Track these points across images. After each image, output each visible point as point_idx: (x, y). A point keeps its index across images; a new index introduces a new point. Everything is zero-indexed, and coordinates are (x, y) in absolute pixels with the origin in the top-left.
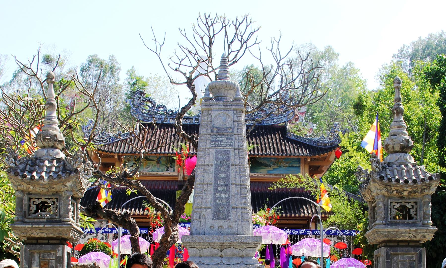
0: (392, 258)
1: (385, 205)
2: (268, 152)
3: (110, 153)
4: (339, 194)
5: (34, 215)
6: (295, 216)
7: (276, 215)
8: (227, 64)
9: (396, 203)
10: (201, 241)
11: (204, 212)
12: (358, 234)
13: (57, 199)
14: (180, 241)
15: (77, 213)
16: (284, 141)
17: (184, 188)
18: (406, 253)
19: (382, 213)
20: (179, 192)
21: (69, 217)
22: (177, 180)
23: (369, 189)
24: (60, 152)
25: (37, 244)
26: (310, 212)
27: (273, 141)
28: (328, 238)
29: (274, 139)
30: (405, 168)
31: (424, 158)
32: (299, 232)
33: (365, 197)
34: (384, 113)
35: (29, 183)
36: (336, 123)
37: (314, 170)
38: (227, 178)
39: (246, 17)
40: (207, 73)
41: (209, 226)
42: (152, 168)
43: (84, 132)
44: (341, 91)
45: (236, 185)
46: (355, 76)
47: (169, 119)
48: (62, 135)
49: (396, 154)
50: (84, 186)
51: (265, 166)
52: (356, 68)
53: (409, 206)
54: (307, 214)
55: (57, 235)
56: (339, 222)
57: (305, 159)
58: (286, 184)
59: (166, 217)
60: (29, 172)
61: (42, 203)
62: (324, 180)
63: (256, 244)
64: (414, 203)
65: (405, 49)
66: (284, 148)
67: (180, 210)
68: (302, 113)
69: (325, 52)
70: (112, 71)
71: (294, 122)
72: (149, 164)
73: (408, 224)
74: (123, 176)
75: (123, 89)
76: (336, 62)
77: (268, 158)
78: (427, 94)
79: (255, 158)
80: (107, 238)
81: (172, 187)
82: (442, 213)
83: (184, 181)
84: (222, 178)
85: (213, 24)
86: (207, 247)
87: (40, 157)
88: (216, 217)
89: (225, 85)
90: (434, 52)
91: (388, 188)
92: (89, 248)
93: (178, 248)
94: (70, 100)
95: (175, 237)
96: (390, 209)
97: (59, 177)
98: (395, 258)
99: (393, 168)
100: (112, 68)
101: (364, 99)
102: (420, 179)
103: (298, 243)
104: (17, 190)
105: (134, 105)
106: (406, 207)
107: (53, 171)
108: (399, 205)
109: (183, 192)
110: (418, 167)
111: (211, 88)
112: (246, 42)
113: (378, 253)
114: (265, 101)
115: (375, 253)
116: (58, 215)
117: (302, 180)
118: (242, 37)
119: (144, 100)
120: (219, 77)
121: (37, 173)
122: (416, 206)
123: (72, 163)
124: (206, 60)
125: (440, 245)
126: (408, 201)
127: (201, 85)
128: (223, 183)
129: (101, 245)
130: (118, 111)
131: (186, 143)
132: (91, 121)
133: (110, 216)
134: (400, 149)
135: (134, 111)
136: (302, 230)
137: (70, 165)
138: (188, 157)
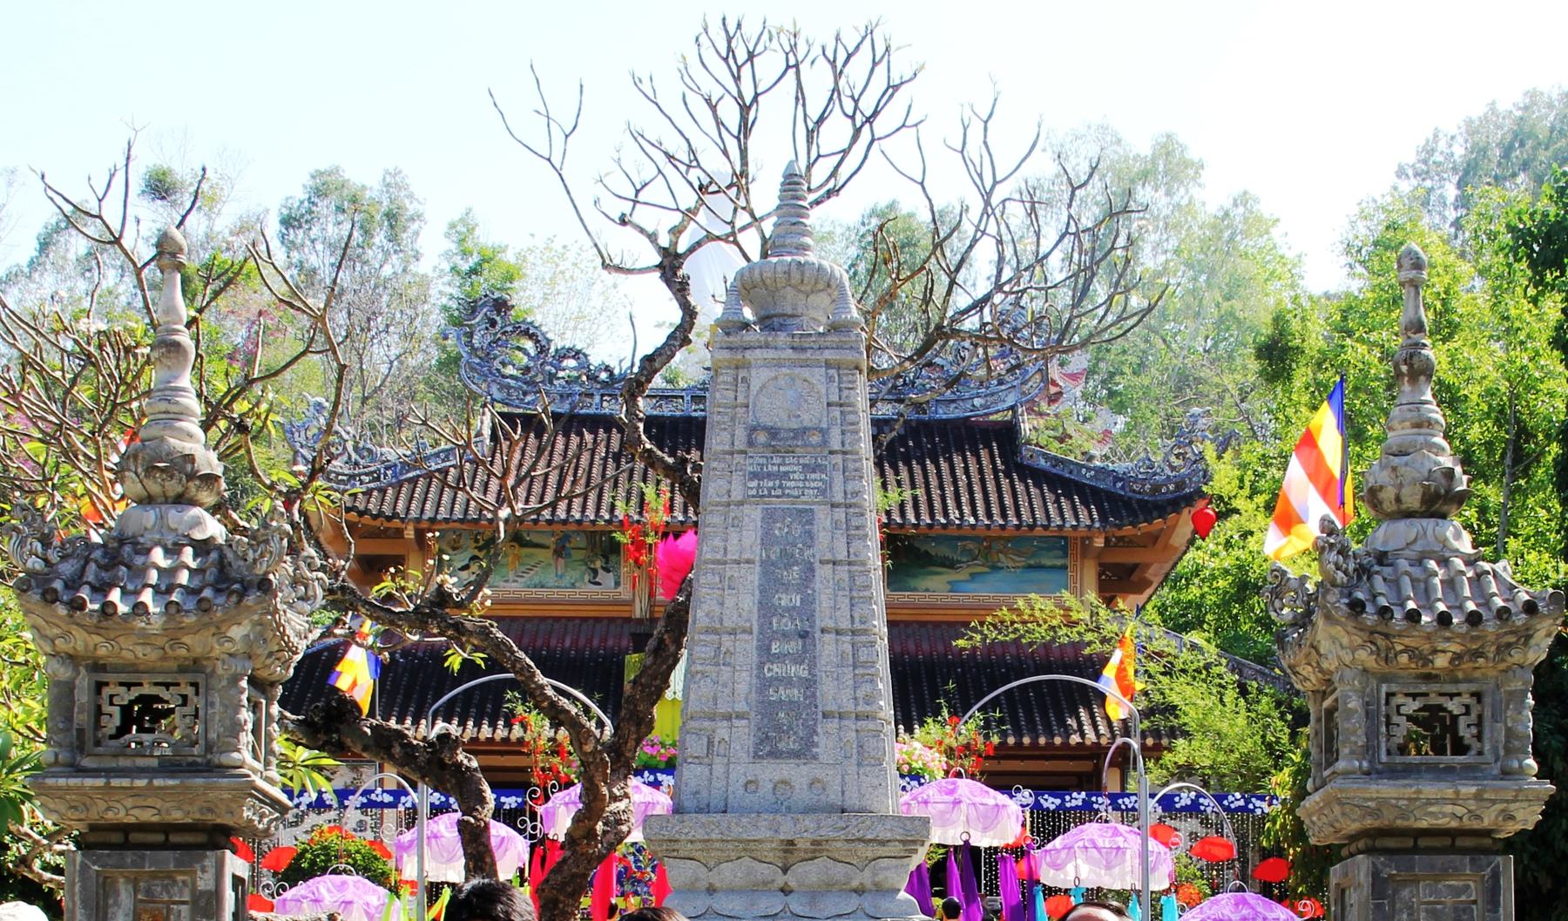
0: (1396, 892)
2: (954, 514)
3: (389, 519)
4: (1207, 667)
5: (113, 743)
6: (1050, 745)
7: (981, 739)
8: (804, 199)
9: (1407, 695)
10: (714, 836)
11: (722, 731)
13: (195, 685)
15: (268, 735)
16: (1008, 475)
17: (652, 643)
18: (1444, 874)
19: (1360, 732)
21: (238, 750)
22: (626, 615)
23: (1312, 646)
24: (207, 516)
25: (126, 846)
27: (969, 477)
28: (1168, 822)
29: (973, 468)
30: (1441, 572)
31: (1508, 534)
32: (1064, 801)
35: (97, 630)
36: (1196, 410)
37: (1118, 581)
38: (807, 609)
40: (733, 234)
41: (742, 781)
42: (537, 576)
43: (292, 447)
44: (1211, 297)
45: (838, 632)
46: (1261, 242)
47: (597, 399)
48: (213, 456)
50: (295, 640)
51: (944, 566)
52: (1266, 216)
53: (1454, 706)
54: (1091, 736)
55: (198, 816)
58: (1016, 630)
59: (588, 748)
60: (94, 589)
62: (1151, 614)
63: (910, 844)
64: (1473, 694)
65: (1442, 145)
66: (1008, 501)
67: (638, 725)
68: (1074, 377)
70: (392, 227)
71: (1044, 407)
73: (1450, 770)
74: (432, 604)
77: (955, 536)
78: (1517, 306)
79: (907, 538)
81: (610, 643)
83: (653, 620)
84: (788, 609)
85: (751, 56)
86: (733, 855)
87: (134, 537)
88: (767, 747)
89: (796, 276)
90: (1543, 156)
91: (1381, 642)
92: (313, 863)
93: (631, 858)
94: (243, 332)
95: (619, 822)
96: (1388, 717)
97: (204, 607)
98: (1405, 893)
99: (1396, 571)
100: (391, 217)
101: (1295, 325)
102: (1494, 609)
103: (1058, 842)
106: (1445, 710)
107: (181, 586)
108: (1416, 705)
109: (649, 661)
110: (1487, 566)
111: (745, 287)
113: (1346, 875)
114: (939, 334)
115: (1335, 874)
116: (202, 742)
118: (856, 102)
119: (509, 329)
121: (124, 592)
124: (729, 187)
127: (713, 275)
128: (790, 627)
129: (358, 852)
130: (418, 370)
132: (319, 407)
133: (386, 745)
134: (1423, 502)
135: (473, 369)
136: (1075, 795)
137: (241, 563)
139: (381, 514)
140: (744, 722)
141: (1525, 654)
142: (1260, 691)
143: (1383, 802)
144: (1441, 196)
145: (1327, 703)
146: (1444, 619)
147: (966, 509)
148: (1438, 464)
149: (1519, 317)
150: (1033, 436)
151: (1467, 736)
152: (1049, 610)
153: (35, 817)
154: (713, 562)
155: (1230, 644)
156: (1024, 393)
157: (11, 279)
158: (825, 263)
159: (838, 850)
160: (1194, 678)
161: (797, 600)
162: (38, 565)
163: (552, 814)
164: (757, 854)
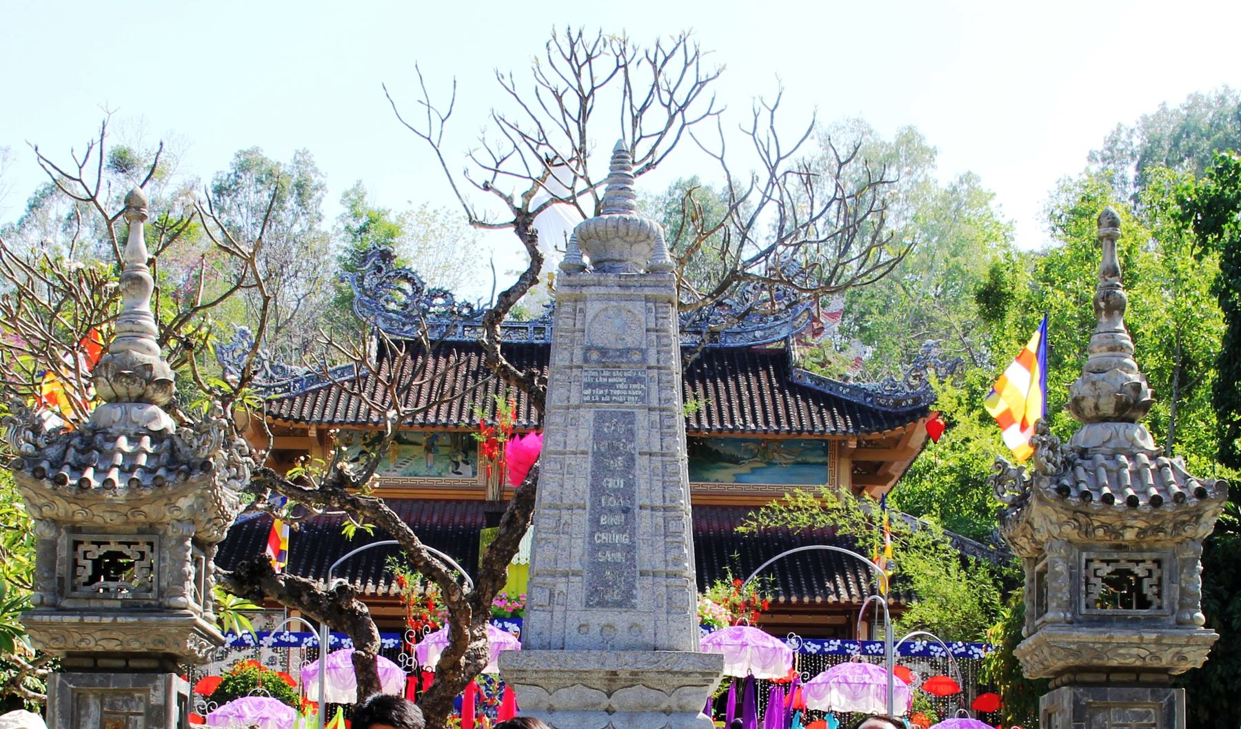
0: (1092, 716)
1: (1071, 568)
2: (739, 422)
3: (297, 421)
4: (935, 544)
5: (87, 588)
6: (812, 603)
7: (758, 598)
8: (630, 169)
9: (1102, 561)
10: (554, 668)
11: (561, 585)
12: (990, 653)
13: (151, 544)
14: (492, 669)
15: (207, 584)
16: (782, 392)
17: (505, 518)
18: (1131, 702)
19: (1065, 590)
20: (486, 531)
21: (184, 596)
22: (481, 498)
23: (1028, 522)
24: (162, 413)
25: (95, 669)
26: (854, 591)
27: (750, 393)
28: (905, 664)
29: (754, 386)
30: (1130, 465)
31: (1175, 441)
32: (823, 646)
33: (1014, 544)
34: (1064, 316)
35: (75, 500)
36: (930, 341)
37: (867, 475)
38: (628, 491)
39: (682, 40)
40: (573, 197)
41: (577, 624)
42: (411, 466)
43: (221, 364)
44: (941, 254)
45: (653, 509)
46: (981, 211)
47: (460, 329)
48: (167, 366)
49: (1104, 425)
50: (228, 509)
51: (730, 461)
52: (985, 190)
53: (1139, 570)
54: (845, 597)
55: (152, 646)
56: (936, 620)
57: (840, 442)
58: (784, 518)
59: (455, 598)
60: (73, 468)
61: (108, 554)
62: (891, 502)
63: (708, 676)
64: (1155, 561)
65: (1123, 136)
66: (781, 411)
67: (494, 581)
68: (833, 316)
69: (898, 144)
70: (300, 195)
71: (809, 339)
72: (402, 454)
73: (1136, 620)
74: (334, 484)
75: (331, 246)
76: (929, 172)
77: (739, 439)
78: (1185, 260)
79: (702, 439)
80: (286, 662)
81: (468, 520)
82: (1226, 597)
83: (503, 503)
84: (614, 490)
85: (589, 58)
86: (569, 683)
87: (104, 428)
88: (596, 598)
89: (623, 230)
90: (1205, 144)
91: (1082, 519)
92: (235, 689)
93: (483, 688)
94: (184, 276)
95: (478, 657)
96: (1087, 579)
97: (159, 483)
98: (1099, 717)
99: (1094, 463)
100: (300, 186)
101: (1007, 276)
102: (1172, 494)
103: (819, 678)
104: (40, 520)
105: (363, 287)
106: (1132, 573)
107: (140, 466)
108: (1109, 569)
109: (503, 531)
110: (1166, 460)
111: (584, 238)
112: (681, 109)
113: (1052, 702)
114: (736, 276)
115: (1044, 701)
116: (155, 589)
117: (830, 506)
118: (671, 94)
119: (392, 274)
120: (605, 206)
121: (97, 471)
122: (1159, 572)
123: (195, 443)
124: (570, 161)
125: (1221, 688)
126: (1138, 556)
127: (557, 229)
128: (615, 504)
129: (270, 681)
130: (319, 306)
131: (507, 394)
132: (244, 334)
133: (296, 594)
134: (1116, 409)
135: (363, 305)
136: (832, 642)
137: (188, 449)
138: (513, 436)
139: (290, 417)
140: (578, 579)
141: (1196, 530)
142: (978, 564)
143: (1083, 645)
144: (1122, 177)
145: (1039, 567)
146: (1132, 502)
147: (749, 418)
148: (1129, 379)
149: (1184, 271)
150: (801, 361)
151: (1150, 594)
152: (814, 501)
153: (25, 647)
154: (555, 453)
155: (953, 524)
156: (794, 328)
157: (7, 232)
158: (646, 220)
159: (651, 679)
160: (925, 553)
161: (621, 483)
162: (30, 449)
163: (425, 652)
164: (588, 682)
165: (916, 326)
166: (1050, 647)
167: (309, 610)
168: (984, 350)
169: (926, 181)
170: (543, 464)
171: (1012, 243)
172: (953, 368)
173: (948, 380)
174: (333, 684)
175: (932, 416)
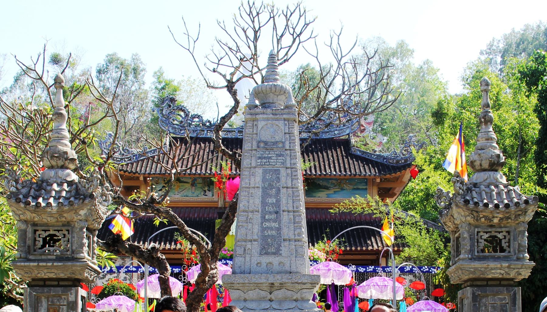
0: (480, 300)
2: (328, 171)
3: (134, 173)
5: (40, 250)
6: (362, 250)
7: (338, 248)
8: (276, 63)
9: (484, 232)
10: (246, 282)
11: (249, 246)
13: (68, 231)
14: (220, 282)
15: (93, 247)
16: (347, 158)
17: (224, 216)
18: (497, 293)
19: (468, 245)
20: (218, 221)
21: (83, 253)
23: (451, 216)
24: (72, 173)
25: (45, 286)
26: (380, 244)
27: (333, 158)
28: (402, 276)
29: (335, 155)
30: (496, 190)
31: (519, 177)
32: (366, 269)
35: (34, 212)
36: (411, 135)
38: (278, 204)
40: (252, 75)
41: (256, 262)
42: (185, 193)
43: (101, 149)
44: (416, 96)
45: (288, 212)
46: (434, 77)
47: (206, 132)
49: (484, 172)
50: (102, 215)
52: (435, 68)
53: (500, 236)
54: (376, 247)
55: (69, 275)
57: (373, 179)
59: (203, 252)
60: (33, 198)
61: (49, 235)
64: (507, 232)
65: (495, 43)
66: (347, 166)
67: (220, 244)
68: (369, 124)
69: (397, 48)
70: (135, 73)
71: (359, 134)
72: (181, 187)
73: (499, 258)
74: (149, 202)
75: (149, 96)
76: (410, 59)
77: (328, 178)
78: (522, 98)
79: (312, 179)
81: (210, 216)
84: (271, 204)
85: (258, 14)
88: (264, 251)
89: (273, 89)
91: (475, 214)
92: (109, 291)
94: (84, 110)
95: (214, 277)
96: (478, 240)
97: (71, 204)
98: (484, 300)
99: (480, 190)
100: (135, 70)
101: (445, 105)
102: (514, 202)
103: (364, 283)
105: (163, 114)
106: (497, 237)
107: (63, 197)
108: (487, 235)
109: (224, 222)
110: (511, 188)
111: (256, 93)
112: (298, 36)
113: (463, 294)
114: (323, 109)
115: (460, 294)
116: (70, 250)
118: (294, 29)
119: (175, 108)
120: (266, 79)
121: (44, 199)
124: (250, 59)
125: (540, 284)
126: (500, 230)
127: (244, 89)
128: (272, 210)
129: (124, 288)
132: (110, 135)
133: (133, 251)
134: (489, 166)
135: (163, 122)
136: (370, 267)
137: (84, 189)
138: (229, 179)
139: (132, 172)
140: (256, 243)
143: (476, 269)
145: (457, 235)
146: (497, 206)
147: (333, 169)
150: (355, 144)
151: (505, 246)
153: (14, 276)
154: (245, 188)
156: (352, 129)
158: (284, 85)
160: (411, 226)
165: (406, 128)
166: (461, 270)
167: (139, 258)
168: (435, 137)
169: (410, 64)
170: (240, 192)
171: (447, 91)
172: (421, 146)
173: (421, 151)
174: (150, 289)
175: (413, 167)
